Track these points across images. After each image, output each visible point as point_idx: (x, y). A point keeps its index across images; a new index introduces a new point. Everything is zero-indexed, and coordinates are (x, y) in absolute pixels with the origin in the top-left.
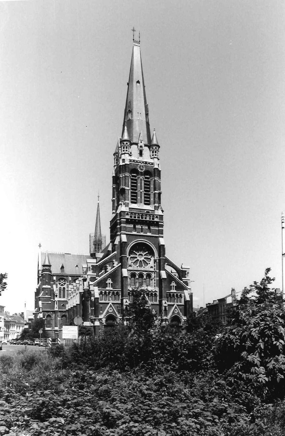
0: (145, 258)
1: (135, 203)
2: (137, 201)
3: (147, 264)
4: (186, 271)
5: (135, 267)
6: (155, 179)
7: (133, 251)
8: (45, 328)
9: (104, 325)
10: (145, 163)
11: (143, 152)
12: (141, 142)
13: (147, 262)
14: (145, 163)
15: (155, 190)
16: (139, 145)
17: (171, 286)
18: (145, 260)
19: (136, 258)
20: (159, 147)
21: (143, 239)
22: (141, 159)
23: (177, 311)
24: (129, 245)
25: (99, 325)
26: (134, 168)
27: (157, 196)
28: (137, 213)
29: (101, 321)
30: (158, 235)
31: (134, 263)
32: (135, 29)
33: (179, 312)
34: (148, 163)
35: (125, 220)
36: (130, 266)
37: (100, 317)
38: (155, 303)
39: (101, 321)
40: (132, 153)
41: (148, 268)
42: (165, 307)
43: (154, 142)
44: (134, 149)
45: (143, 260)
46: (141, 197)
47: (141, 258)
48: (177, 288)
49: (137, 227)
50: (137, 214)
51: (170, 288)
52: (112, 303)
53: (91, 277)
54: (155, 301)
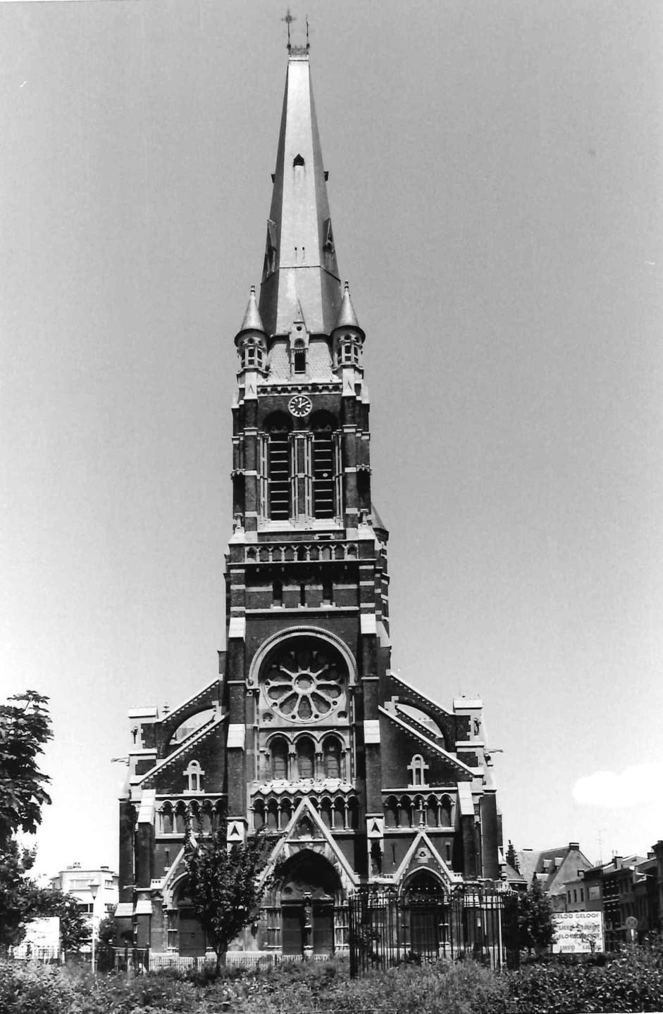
0: (319, 687)
1: (285, 517)
2: (290, 510)
3: (328, 705)
4: (468, 718)
5: (282, 719)
6: (346, 431)
7: (278, 668)
8: (110, 916)
9: (170, 913)
10: (310, 388)
11: (308, 358)
12: (299, 329)
13: (328, 698)
14: (310, 388)
15: (345, 465)
16: (293, 339)
17: (411, 770)
18: (319, 692)
19: (290, 688)
20: (361, 335)
21: (319, 625)
22: (300, 379)
23: (429, 855)
24: (259, 650)
25: (150, 911)
26: (276, 408)
27: (352, 482)
28: (282, 545)
29: (158, 899)
30: (356, 608)
31: (282, 705)
32: (292, 14)
33: (435, 858)
34: (320, 387)
35: (243, 571)
36: (268, 715)
37: (154, 886)
38: (443, 829)
39: (158, 899)
40: (272, 366)
41: (330, 718)
42: (375, 841)
43: (348, 319)
44: (278, 358)
45: (314, 695)
46: (301, 495)
47: (306, 688)
48: (430, 777)
49: (285, 588)
50: (283, 549)
51: (408, 778)
52: (429, 835)
53: (139, 761)
54: (444, 825)
